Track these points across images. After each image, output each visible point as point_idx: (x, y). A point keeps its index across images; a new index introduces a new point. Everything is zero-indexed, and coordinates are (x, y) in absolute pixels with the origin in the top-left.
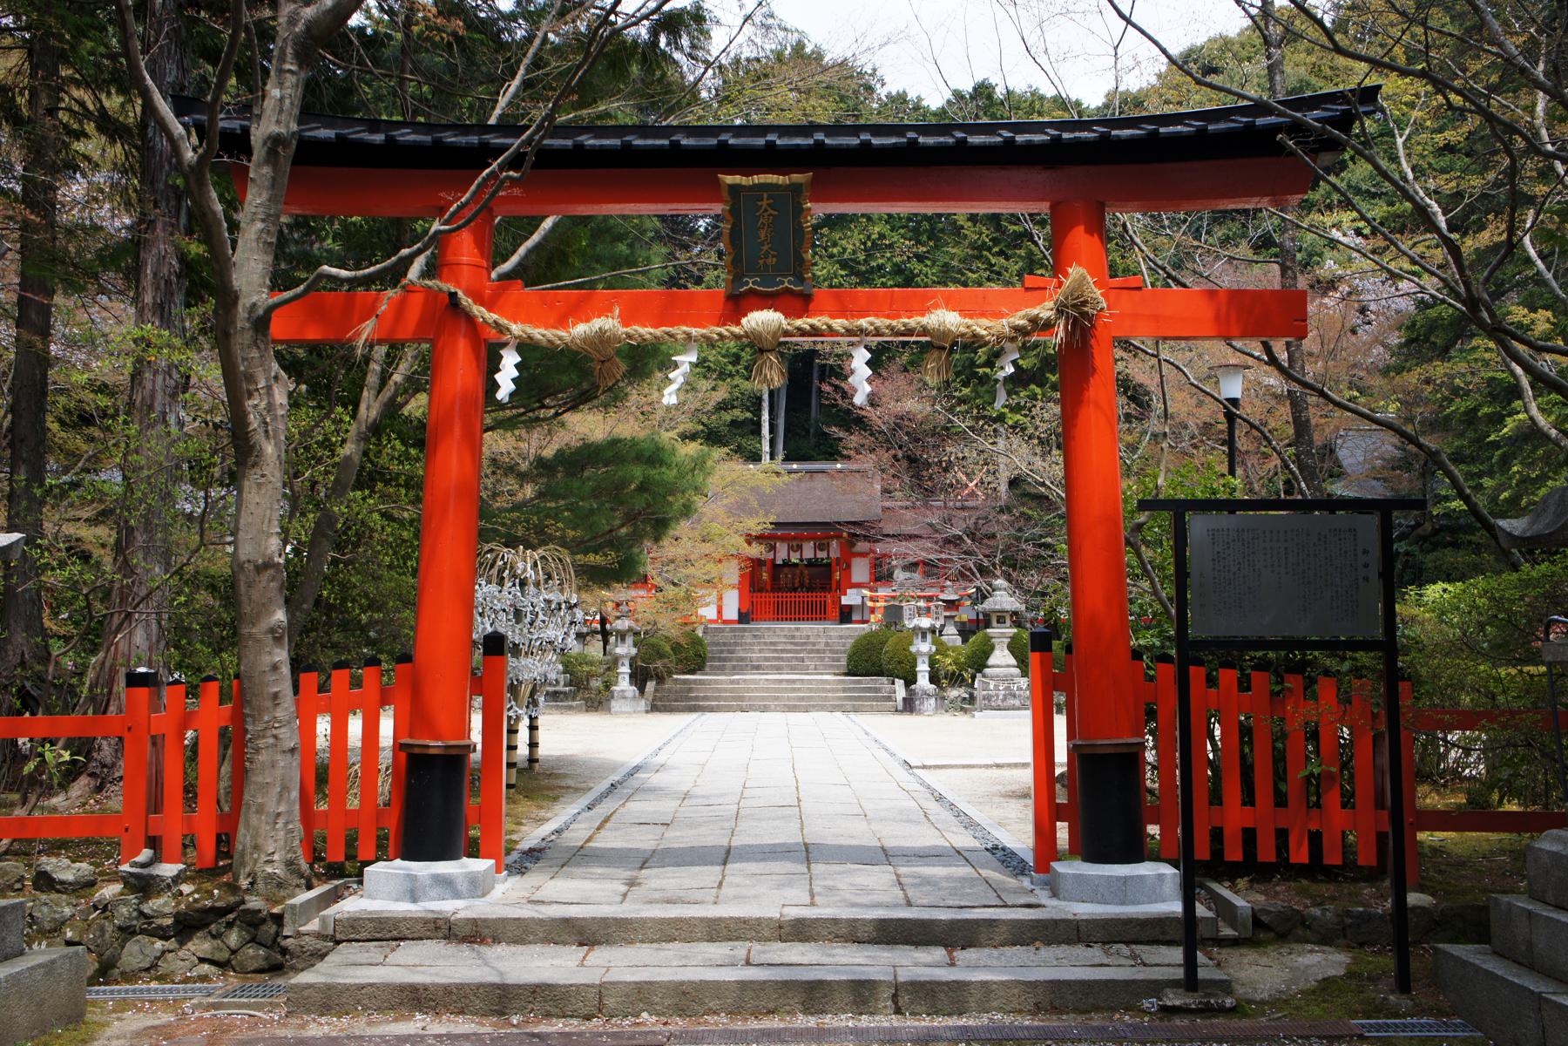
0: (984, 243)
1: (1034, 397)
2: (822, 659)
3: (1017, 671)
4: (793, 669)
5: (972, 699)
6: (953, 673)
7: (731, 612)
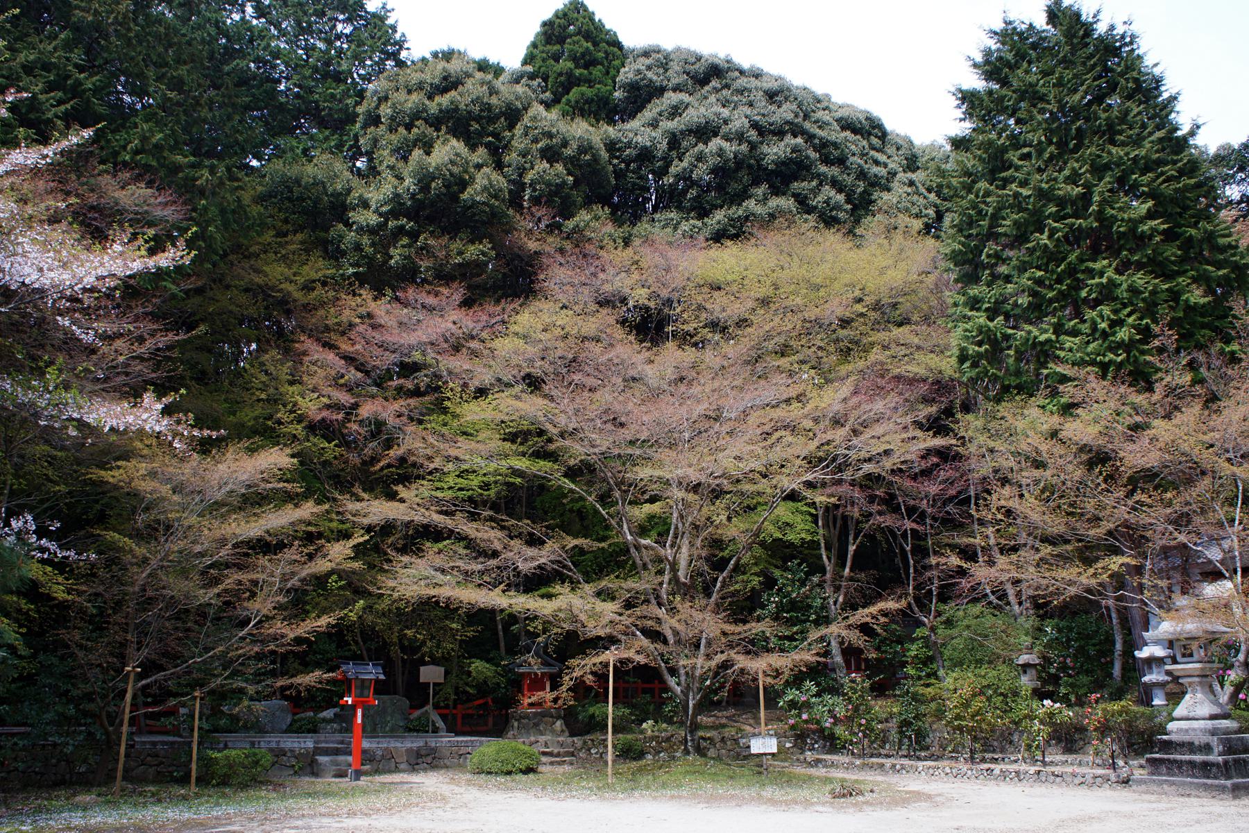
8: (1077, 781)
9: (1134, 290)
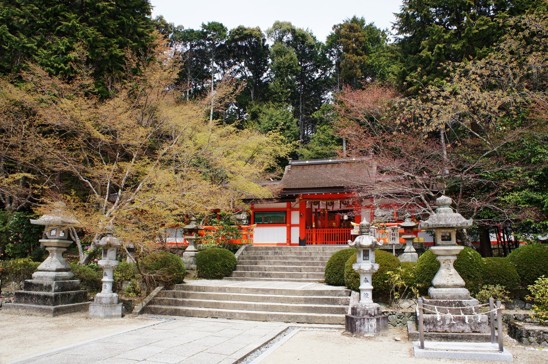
1: (451, 325)
2: (314, 270)
3: (465, 292)
6: (403, 287)
7: (295, 239)
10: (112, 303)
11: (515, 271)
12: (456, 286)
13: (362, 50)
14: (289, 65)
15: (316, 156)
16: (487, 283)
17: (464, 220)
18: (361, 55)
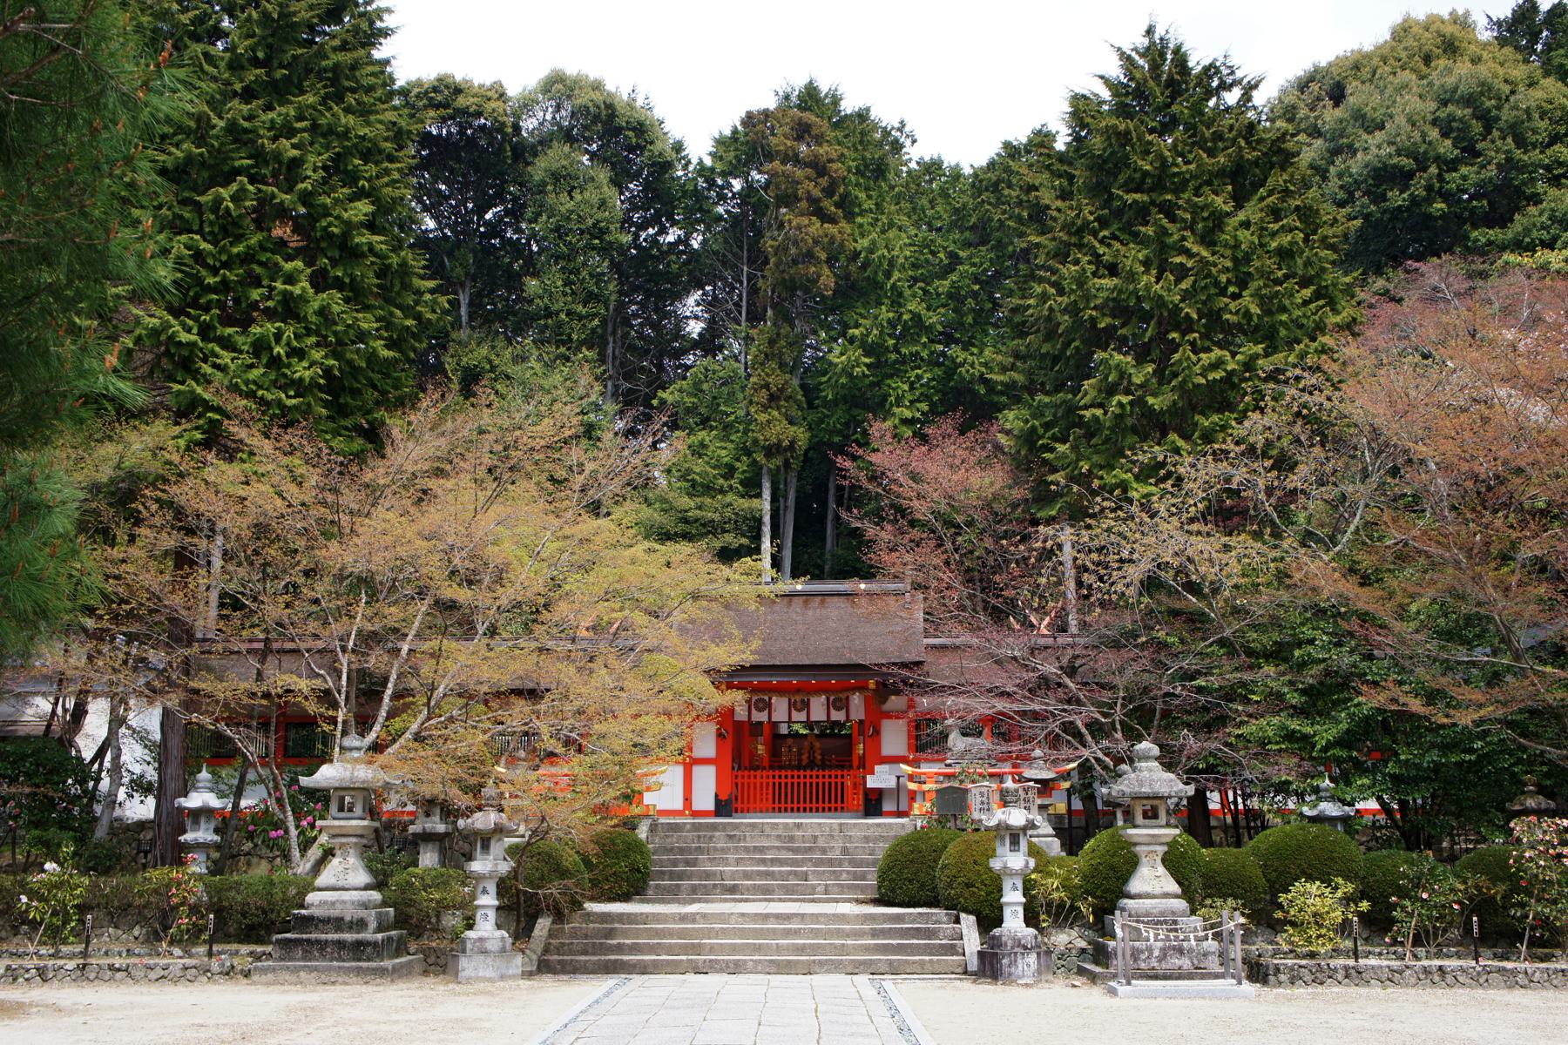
0: (1087, 224)
2: (836, 875)
3: (1181, 904)
4: (790, 892)
5: (1101, 955)
6: (1061, 905)
7: (705, 798)
8: (153, 975)
9: (323, 312)
10: (503, 950)
11: (1259, 872)
12: (1166, 895)
13: (837, 205)
14: (594, 225)
15: (681, 527)
16: (1210, 896)
17: (1181, 786)
18: (833, 221)
